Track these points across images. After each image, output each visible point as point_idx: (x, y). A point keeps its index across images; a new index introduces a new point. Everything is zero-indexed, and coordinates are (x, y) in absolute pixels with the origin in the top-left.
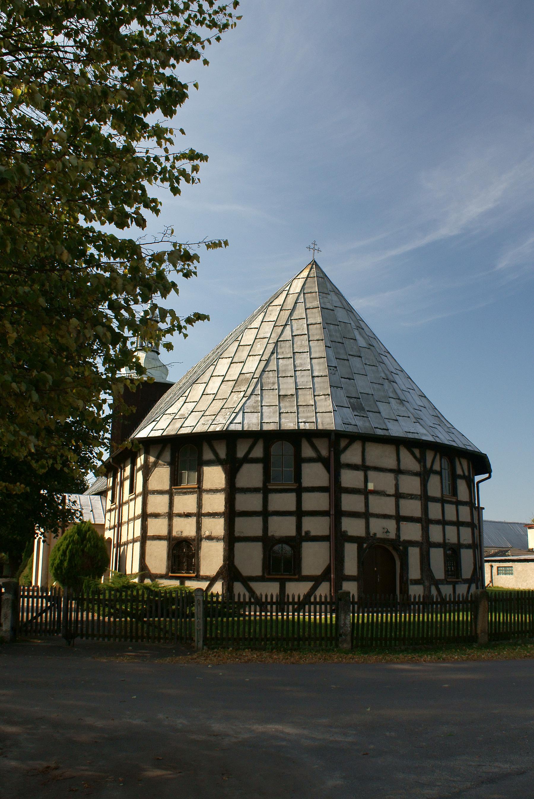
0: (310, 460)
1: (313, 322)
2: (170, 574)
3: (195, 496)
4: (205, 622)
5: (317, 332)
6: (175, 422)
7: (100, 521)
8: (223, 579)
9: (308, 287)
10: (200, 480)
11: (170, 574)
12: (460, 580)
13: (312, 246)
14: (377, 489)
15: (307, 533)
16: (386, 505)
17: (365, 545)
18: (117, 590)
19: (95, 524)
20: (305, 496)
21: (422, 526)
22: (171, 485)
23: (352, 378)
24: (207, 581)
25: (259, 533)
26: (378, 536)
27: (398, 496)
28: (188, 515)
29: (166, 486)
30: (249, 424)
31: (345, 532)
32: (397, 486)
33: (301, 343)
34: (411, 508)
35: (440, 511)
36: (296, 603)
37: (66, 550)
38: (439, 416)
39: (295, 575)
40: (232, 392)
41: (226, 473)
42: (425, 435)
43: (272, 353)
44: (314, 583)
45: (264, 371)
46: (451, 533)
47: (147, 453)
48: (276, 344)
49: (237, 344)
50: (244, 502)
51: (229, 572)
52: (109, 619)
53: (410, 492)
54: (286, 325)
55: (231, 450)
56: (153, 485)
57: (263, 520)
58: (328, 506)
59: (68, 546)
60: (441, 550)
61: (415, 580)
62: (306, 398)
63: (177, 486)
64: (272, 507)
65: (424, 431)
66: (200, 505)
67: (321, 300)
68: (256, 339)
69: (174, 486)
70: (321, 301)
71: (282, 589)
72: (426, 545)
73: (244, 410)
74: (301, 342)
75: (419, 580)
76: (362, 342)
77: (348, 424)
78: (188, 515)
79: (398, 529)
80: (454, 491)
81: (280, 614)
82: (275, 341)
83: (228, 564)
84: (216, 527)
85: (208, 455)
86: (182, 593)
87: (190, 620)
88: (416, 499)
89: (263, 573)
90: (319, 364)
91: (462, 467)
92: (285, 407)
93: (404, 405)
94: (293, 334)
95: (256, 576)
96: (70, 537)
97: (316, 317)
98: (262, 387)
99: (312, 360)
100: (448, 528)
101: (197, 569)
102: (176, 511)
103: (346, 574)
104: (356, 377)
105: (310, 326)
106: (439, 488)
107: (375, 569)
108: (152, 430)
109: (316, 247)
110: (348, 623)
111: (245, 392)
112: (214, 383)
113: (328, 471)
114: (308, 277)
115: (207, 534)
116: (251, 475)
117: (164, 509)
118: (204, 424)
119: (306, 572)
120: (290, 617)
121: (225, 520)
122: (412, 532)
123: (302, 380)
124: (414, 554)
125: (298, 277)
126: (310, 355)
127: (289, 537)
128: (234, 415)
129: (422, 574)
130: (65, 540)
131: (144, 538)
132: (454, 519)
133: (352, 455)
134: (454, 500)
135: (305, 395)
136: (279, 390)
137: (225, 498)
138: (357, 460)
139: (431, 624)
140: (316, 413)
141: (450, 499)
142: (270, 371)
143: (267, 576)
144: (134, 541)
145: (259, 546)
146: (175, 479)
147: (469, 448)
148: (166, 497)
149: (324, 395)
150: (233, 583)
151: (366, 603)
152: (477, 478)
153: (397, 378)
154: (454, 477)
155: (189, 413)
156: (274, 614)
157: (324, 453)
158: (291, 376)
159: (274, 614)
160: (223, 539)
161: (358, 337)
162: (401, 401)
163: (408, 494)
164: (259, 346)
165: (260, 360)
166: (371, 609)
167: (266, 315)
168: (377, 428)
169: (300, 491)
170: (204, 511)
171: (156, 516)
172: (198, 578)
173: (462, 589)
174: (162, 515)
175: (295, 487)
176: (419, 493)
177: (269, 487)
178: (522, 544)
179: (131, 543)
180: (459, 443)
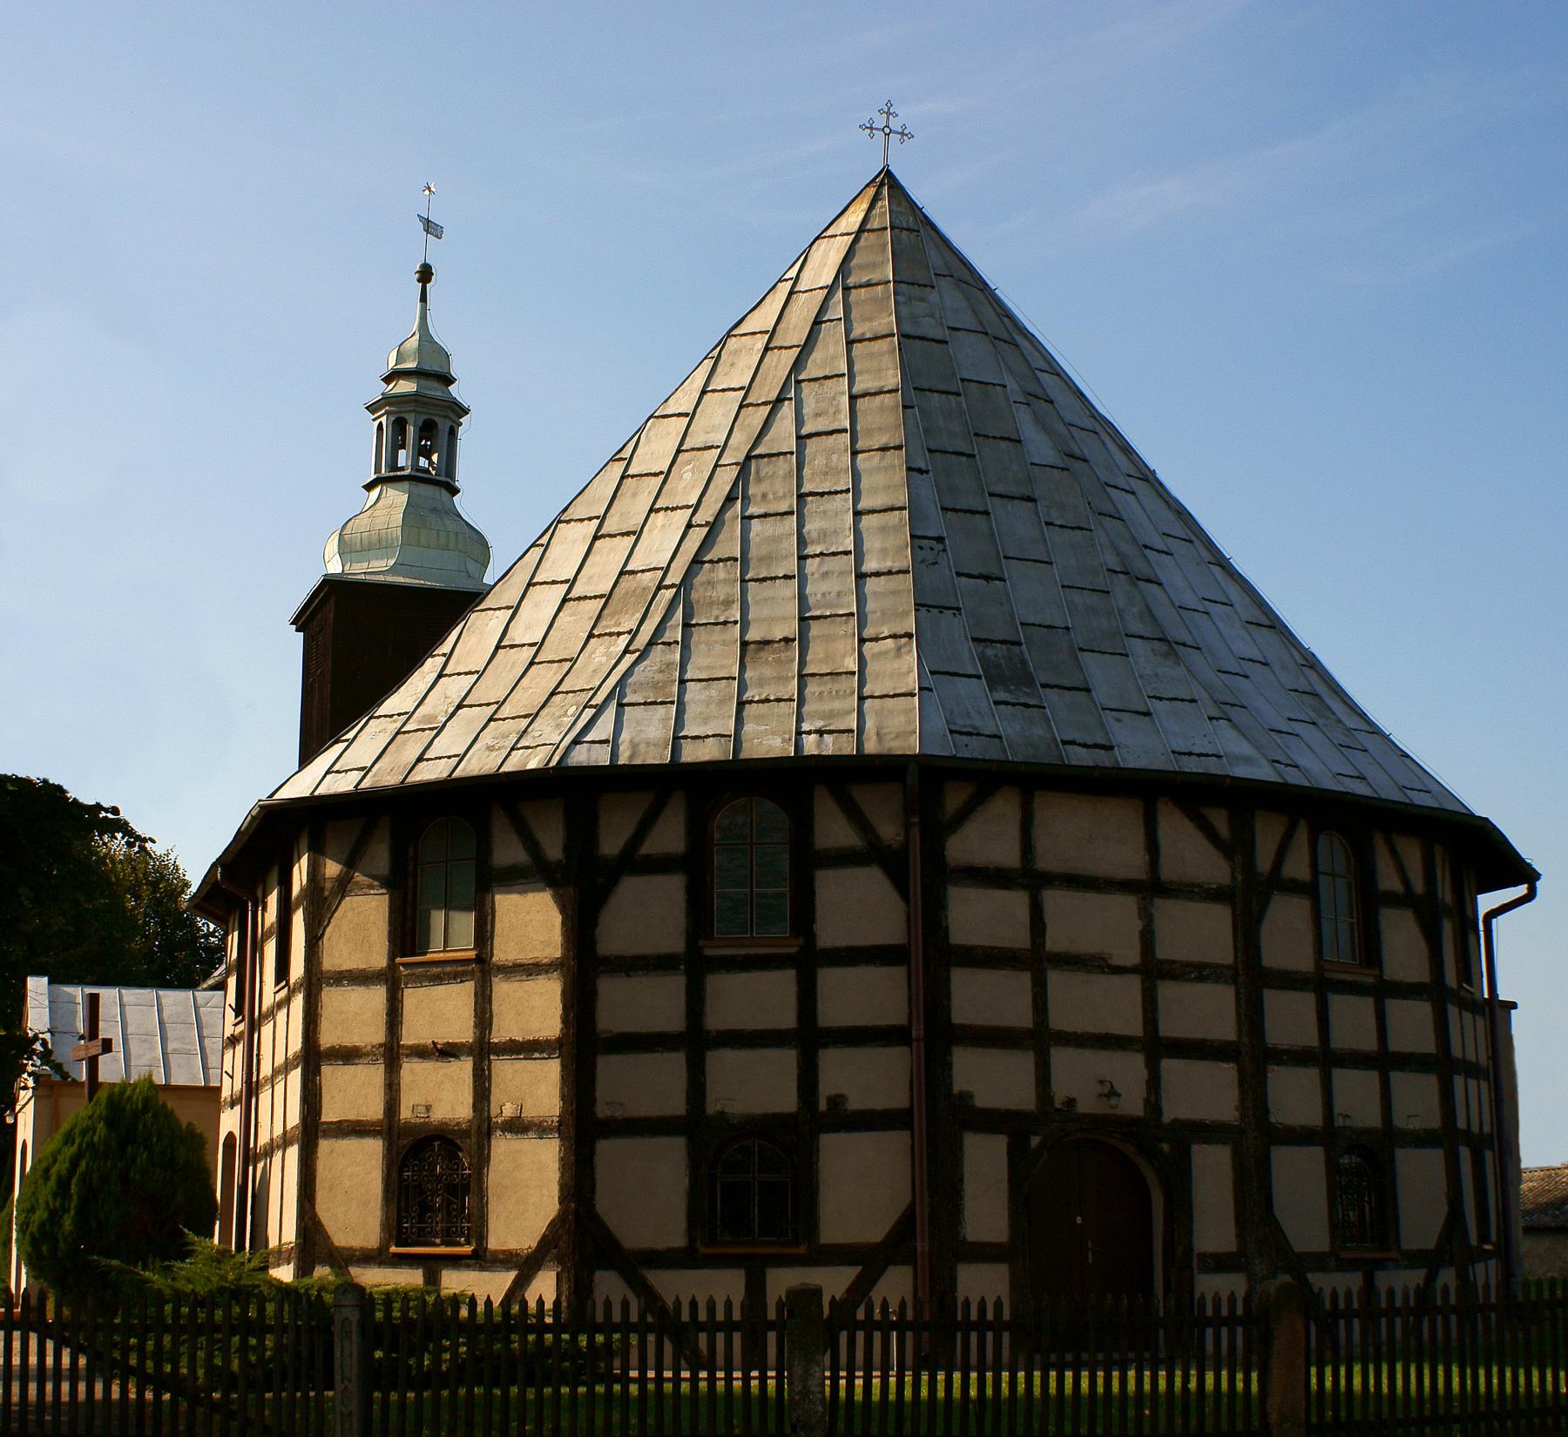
2: (393, 1249)
3: (469, 987)
4: (368, 1402)
5: (883, 421)
6: (404, 743)
7: (187, 1074)
10: (484, 935)
11: (393, 1249)
12: (1393, 1254)
13: (880, 122)
15: (836, 1101)
16: (1113, 1005)
17: (1035, 1141)
18: (198, 1302)
19: (168, 1088)
20: (829, 979)
22: (392, 956)
23: (997, 572)
24: (508, 1269)
25: (676, 1105)
26: (1083, 1107)
27: (1153, 971)
28: (447, 1052)
29: (377, 956)
30: (634, 746)
31: (966, 1096)
32: (1147, 938)
33: (829, 459)
35: (1311, 1016)
37: (70, 1178)
38: (1321, 689)
40: (591, 635)
41: (563, 910)
42: (1248, 760)
43: (730, 499)
44: (1309, 1276)
45: (697, 561)
46: (1357, 1098)
47: (318, 851)
48: (744, 466)
49: (618, 468)
51: (580, 1236)
54: (780, 400)
55: (582, 833)
56: (336, 956)
58: (906, 1010)
59: (74, 1162)
60: (1317, 1154)
61: (1215, 1256)
62: (835, 649)
64: (716, 1020)
66: (484, 1018)
67: (903, 309)
68: (679, 451)
70: (904, 311)
72: (1255, 1138)
73: (622, 695)
74: (829, 458)
75: (1229, 1255)
76: (1040, 448)
77: (968, 734)
78: (447, 1052)
79: (1154, 1082)
80: (1370, 948)
81: (685, 1374)
82: (741, 458)
84: (536, 1088)
85: (508, 852)
86: (405, 1309)
87: (319, 1395)
88: (1216, 981)
89: (692, 1238)
91: (1400, 865)
92: (761, 683)
93: (1178, 659)
94: (804, 432)
95: (670, 1250)
96: (84, 1133)
98: (688, 615)
99: (863, 514)
100: (1343, 1078)
102: (408, 1038)
103: (970, 1238)
104: (1013, 570)
105: (860, 401)
106: (1309, 938)
107: (1079, 1220)
108: (328, 772)
109: (895, 124)
111: (634, 634)
112: (536, 605)
113: (902, 888)
114: (862, 229)
115: (509, 1111)
116: (648, 913)
117: (372, 1033)
118: (490, 749)
120: (737, 1384)
122: (1201, 1092)
124: (1212, 1168)
125: (829, 233)
126: (856, 501)
128: (590, 712)
129: (1240, 1236)
130: (66, 1143)
131: (311, 1131)
132: (1369, 1043)
133: (988, 837)
134: (1370, 980)
136: (745, 624)
137: (564, 993)
138: (1006, 853)
140: (862, 699)
141: (1349, 978)
142: (720, 560)
144: (285, 1142)
145: (675, 1148)
146: (407, 934)
147: (1420, 799)
148: (377, 996)
150: (592, 1273)
151: (1039, 1333)
152: (1486, 902)
153: (1166, 569)
155: (451, 710)
156: (737, 1374)
157: (889, 832)
158: (786, 577)
159: (737, 1374)
160: (559, 1131)
162: (1170, 647)
164: (688, 476)
165: (689, 526)
166: (1053, 1357)
167: (719, 369)
168: (1072, 743)
169: (808, 961)
170: (499, 1035)
171: (348, 1055)
172: (482, 1259)
173: (1402, 1281)
174: (367, 1054)
175: (793, 950)
177: (708, 952)
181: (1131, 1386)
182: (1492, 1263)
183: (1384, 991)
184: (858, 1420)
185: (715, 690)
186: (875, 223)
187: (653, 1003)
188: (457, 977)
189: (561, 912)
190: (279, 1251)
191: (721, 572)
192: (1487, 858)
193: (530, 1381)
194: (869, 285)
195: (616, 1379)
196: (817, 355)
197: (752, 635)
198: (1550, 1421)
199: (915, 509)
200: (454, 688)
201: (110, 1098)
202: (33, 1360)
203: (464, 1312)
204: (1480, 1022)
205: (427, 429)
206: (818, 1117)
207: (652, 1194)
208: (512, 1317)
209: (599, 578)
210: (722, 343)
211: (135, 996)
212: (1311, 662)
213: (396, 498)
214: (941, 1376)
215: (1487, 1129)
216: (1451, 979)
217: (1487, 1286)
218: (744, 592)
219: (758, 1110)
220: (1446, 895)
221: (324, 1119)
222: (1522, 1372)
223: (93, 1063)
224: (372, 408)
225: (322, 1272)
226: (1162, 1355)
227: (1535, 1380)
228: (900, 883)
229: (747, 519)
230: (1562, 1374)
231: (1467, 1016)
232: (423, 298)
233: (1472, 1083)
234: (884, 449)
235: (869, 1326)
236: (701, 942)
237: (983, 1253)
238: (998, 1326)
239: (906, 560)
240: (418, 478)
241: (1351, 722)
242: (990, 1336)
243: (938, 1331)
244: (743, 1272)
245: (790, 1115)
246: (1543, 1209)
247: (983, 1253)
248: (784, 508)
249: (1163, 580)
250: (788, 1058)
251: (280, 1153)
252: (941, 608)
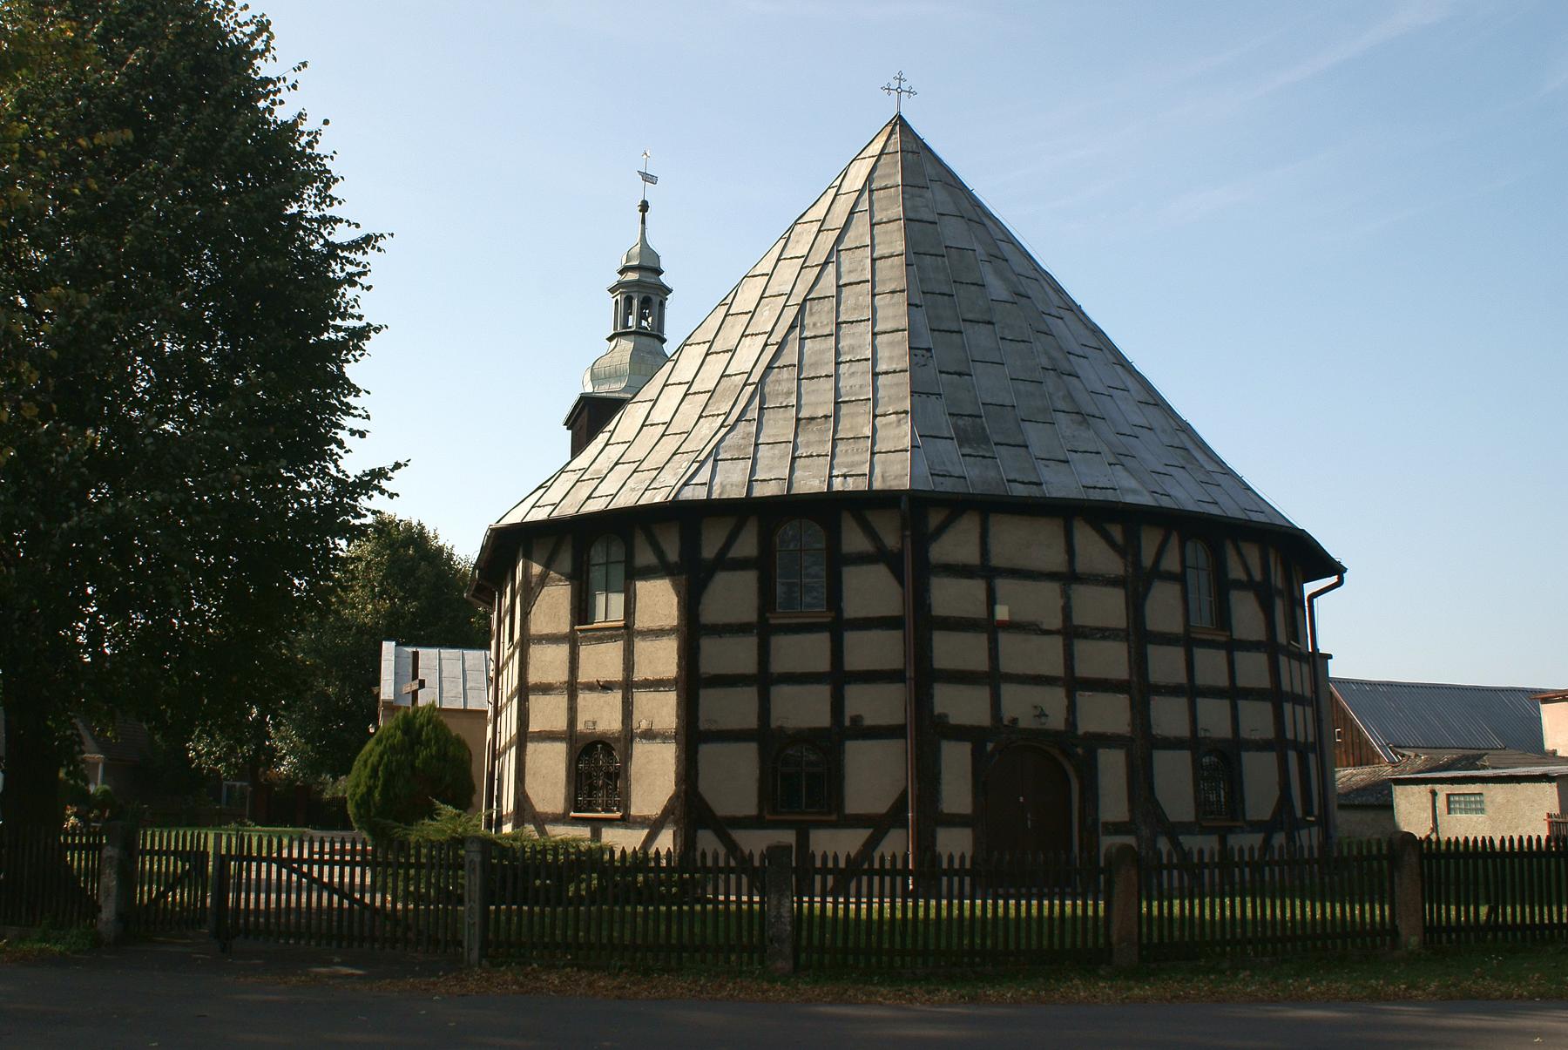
0: (861, 559)
1: (886, 252)
4: (485, 913)
5: (893, 274)
9: (880, 177)
13: (895, 85)
14: (1017, 618)
15: (856, 720)
16: (1046, 656)
17: (990, 747)
18: (440, 846)
21: (1131, 699)
22: (573, 624)
25: (752, 722)
26: (1022, 724)
27: (1071, 633)
28: (606, 687)
30: (723, 486)
32: (1067, 611)
33: (855, 300)
34: (1109, 660)
35: (1182, 664)
36: (865, 872)
38: (1190, 445)
42: (1134, 491)
43: (792, 327)
45: (769, 367)
46: (1215, 718)
47: (528, 557)
48: (802, 307)
49: (723, 309)
51: (689, 807)
52: (405, 905)
53: (1100, 624)
54: (826, 263)
55: (691, 544)
56: (539, 625)
59: (381, 757)
60: (1186, 755)
61: (1114, 824)
62: (857, 422)
64: (778, 665)
65: (1133, 484)
66: (629, 665)
67: (908, 204)
70: (908, 204)
71: (803, 840)
72: (1142, 746)
73: (717, 454)
75: (1124, 823)
76: (997, 289)
78: (606, 687)
79: (1072, 708)
80: (1223, 617)
84: (661, 710)
85: (645, 557)
86: (567, 853)
90: (891, 344)
91: (1243, 562)
92: (808, 444)
95: (746, 818)
97: (893, 241)
98: (762, 402)
99: (878, 333)
100: (1203, 704)
101: (625, 805)
102: (582, 678)
109: (905, 86)
110: (786, 914)
111: (728, 415)
113: (901, 582)
115: (644, 725)
117: (559, 675)
118: (633, 490)
119: (853, 806)
122: (1106, 714)
123: (852, 381)
124: (1112, 767)
126: (873, 326)
129: (1131, 810)
131: (523, 737)
132: (1223, 681)
133: (958, 544)
135: (853, 415)
136: (799, 407)
139: (1000, 924)
140: (873, 454)
143: (768, 817)
145: (750, 751)
146: (582, 610)
147: (1255, 517)
148: (563, 650)
149: (896, 413)
151: (987, 876)
152: (1309, 588)
153: (1080, 366)
154: (1222, 587)
156: (817, 899)
157: (891, 541)
161: (992, 280)
162: (1083, 418)
163: (1097, 629)
165: (766, 345)
169: (838, 627)
170: (638, 676)
171: (546, 689)
172: (626, 821)
176: (1122, 624)
177: (772, 621)
178: (1530, 739)
180: (1231, 509)
181: (1034, 911)
182: (1315, 830)
183: (1233, 646)
184: (1208, 930)
185: (778, 449)
186: (890, 149)
187: (737, 655)
188: (613, 638)
191: (785, 373)
192: (1305, 559)
193: (651, 901)
194: (886, 188)
195: (709, 901)
196: (851, 234)
197: (804, 414)
198: (1319, 944)
199: (912, 331)
200: (614, 452)
201: (406, 715)
202: (358, 880)
203: (607, 857)
204: (1306, 668)
205: (646, 303)
206: (846, 728)
207: (735, 781)
208: (640, 861)
209: (707, 381)
210: (791, 229)
211: (434, 652)
212: (1186, 429)
213: (627, 345)
214: (933, 902)
215: (1311, 739)
216: (1282, 638)
217: (1311, 848)
218: (799, 387)
220: (1278, 580)
222: (1318, 905)
223: (415, 694)
224: (612, 290)
225: (530, 828)
226: (1079, 890)
227: (1328, 910)
228: (898, 575)
229: (802, 339)
230: (1565, 909)
231: (1295, 664)
232: (643, 222)
233: (1299, 709)
234: (893, 292)
235: (882, 873)
237: (954, 821)
238: (961, 873)
239: (905, 364)
240: (639, 333)
241: (1210, 467)
242: (887, 879)
243: (929, 874)
246: (1347, 795)
247: (954, 821)
248: (827, 332)
249: (1080, 373)
250: (824, 691)
252: (928, 394)
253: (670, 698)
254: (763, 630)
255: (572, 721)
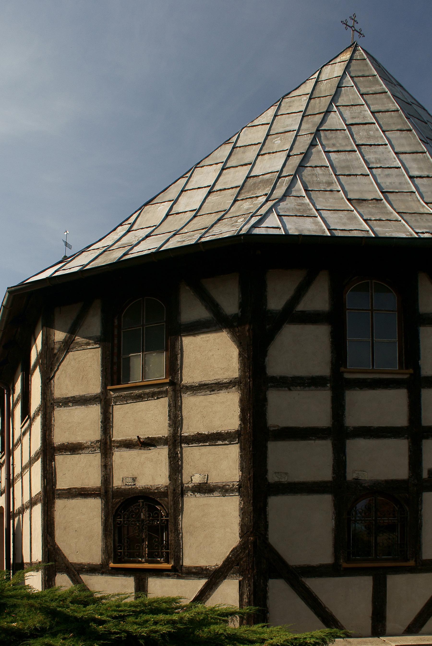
2: (112, 565)
8: (241, 575)
10: (174, 367)
11: (112, 565)
22: (104, 385)
25: (326, 474)
28: (148, 443)
39: (407, 560)
50: (283, 409)
51: (256, 559)
56: (63, 387)
57: (334, 447)
63: (119, 383)
64: (352, 420)
66: (176, 418)
69: (112, 385)
78: (148, 443)
83: (254, 543)
84: (225, 464)
85: (193, 310)
101: (174, 552)
102: (118, 435)
114: (351, 59)
115: (197, 479)
116: (302, 349)
121: (242, 449)
127: (392, 481)
131: (50, 495)
145: (326, 501)
146: (114, 372)
148: (94, 411)
150: (267, 581)
170: (187, 430)
171: (74, 449)
172: (179, 571)
174: (88, 447)
175: (405, 377)
177: (347, 376)
179: (27, 508)
189: (238, 347)
190: (31, 563)
219: (382, 477)
221: (58, 487)
236: (342, 369)
244: (371, 578)
245: (403, 481)
250: (402, 446)
251: (28, 511)
253: (232, 453)
254: (338, 383)
255: (107, 478)
